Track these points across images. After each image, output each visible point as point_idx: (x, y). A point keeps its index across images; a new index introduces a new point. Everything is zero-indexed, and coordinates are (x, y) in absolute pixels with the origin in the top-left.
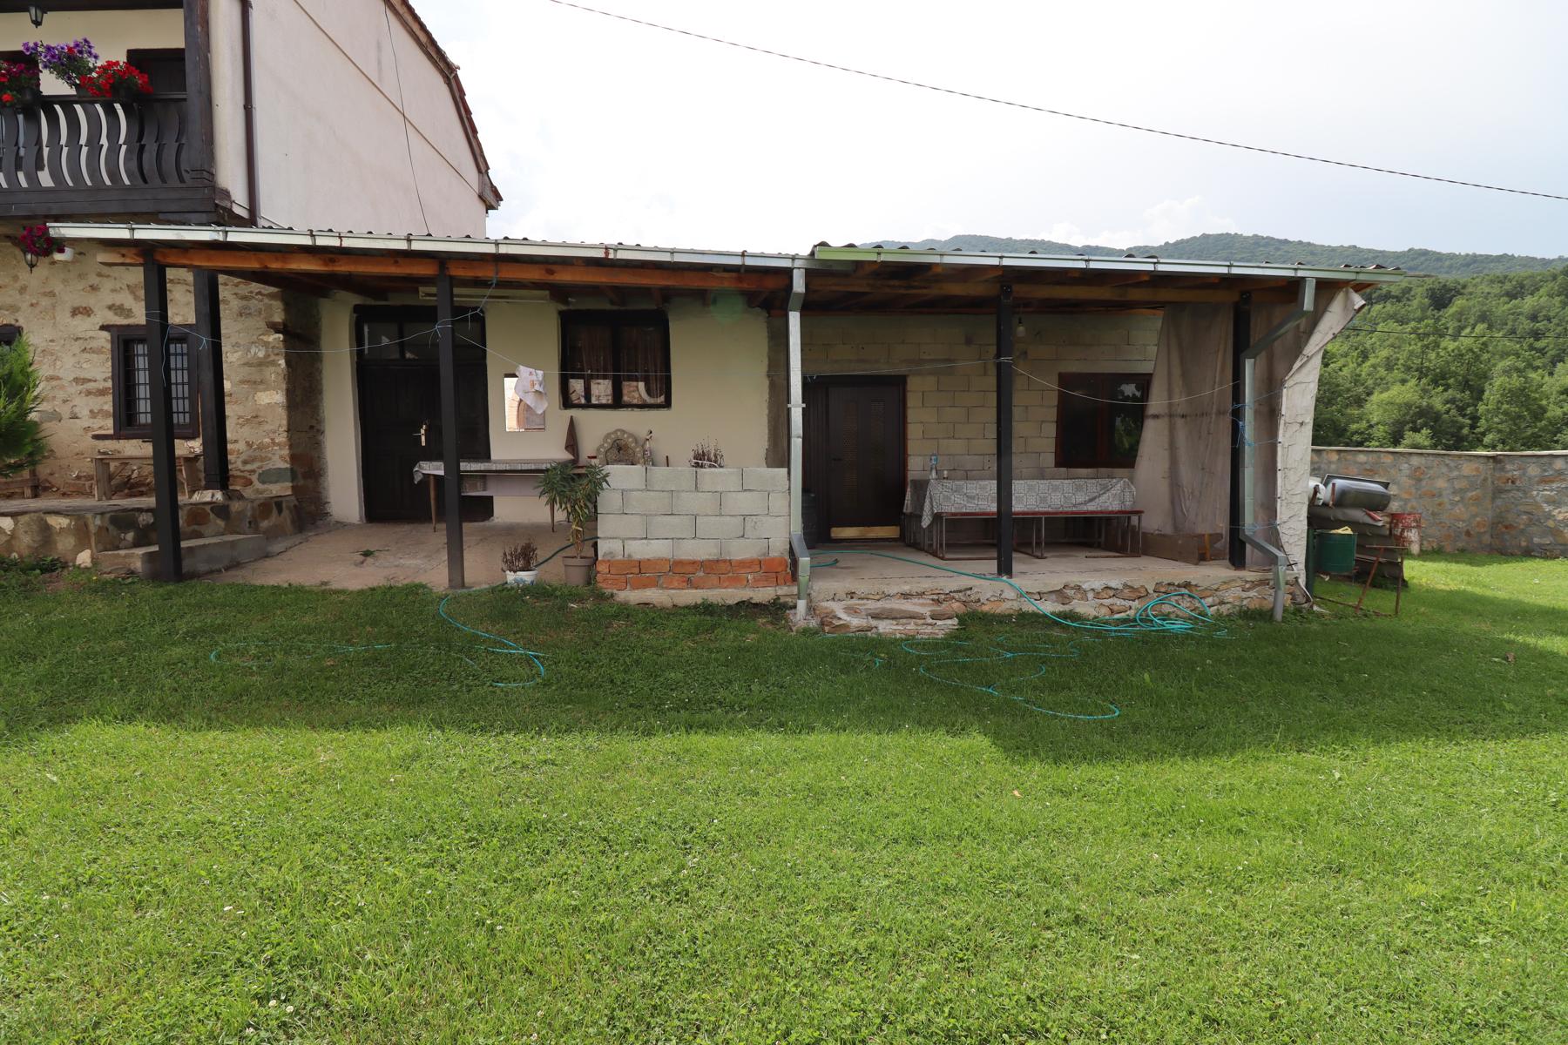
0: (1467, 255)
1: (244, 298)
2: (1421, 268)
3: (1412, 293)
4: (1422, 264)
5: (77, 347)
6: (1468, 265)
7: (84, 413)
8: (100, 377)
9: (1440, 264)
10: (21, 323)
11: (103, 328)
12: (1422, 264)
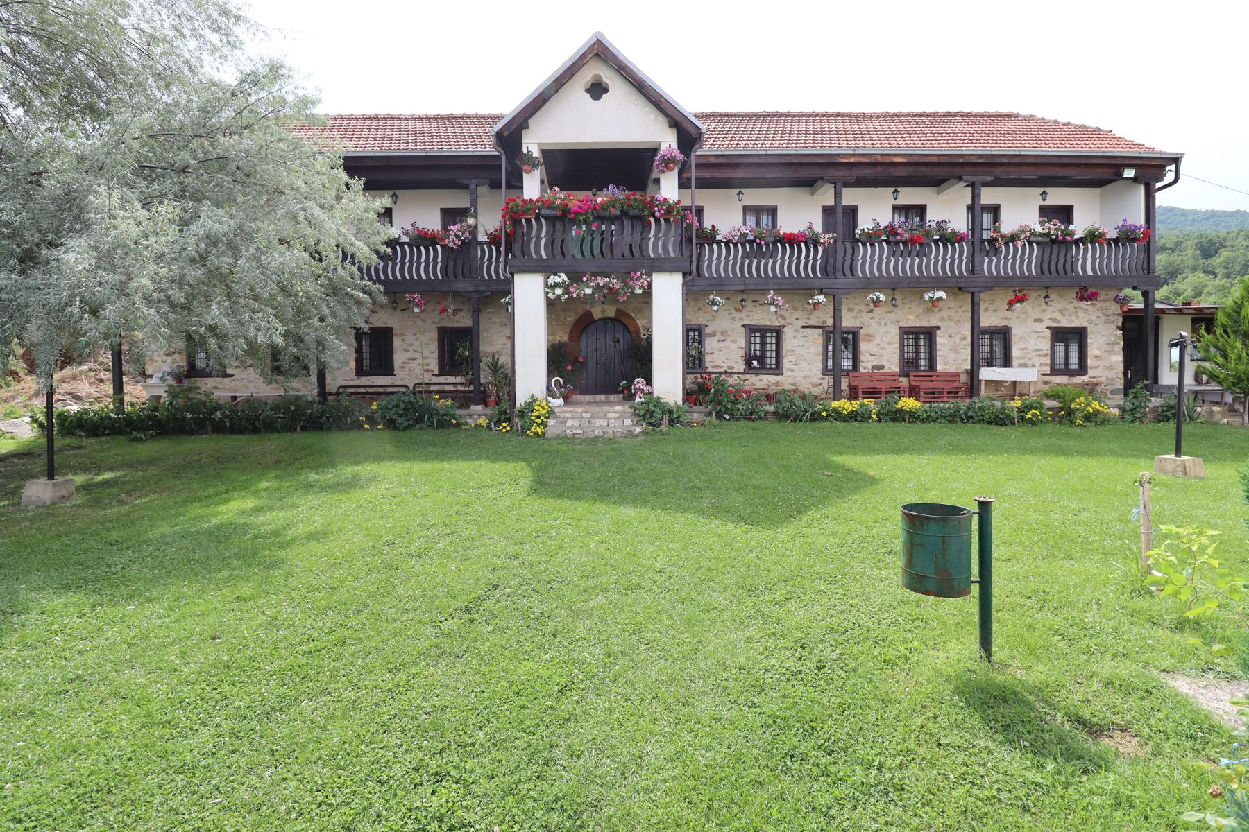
0: (1207, 211)
1: (1106, 315)
2: (1169, 221)
3: (1182, 246)
4: (1169, 218)
5: (1035, 336)
6: (1208, 219)
7: (1037, 364)
8: (1045, 348)
9: (1184, 218)
10: (1012, 325)
11: (1047, 328)
12: (1169, 218)
